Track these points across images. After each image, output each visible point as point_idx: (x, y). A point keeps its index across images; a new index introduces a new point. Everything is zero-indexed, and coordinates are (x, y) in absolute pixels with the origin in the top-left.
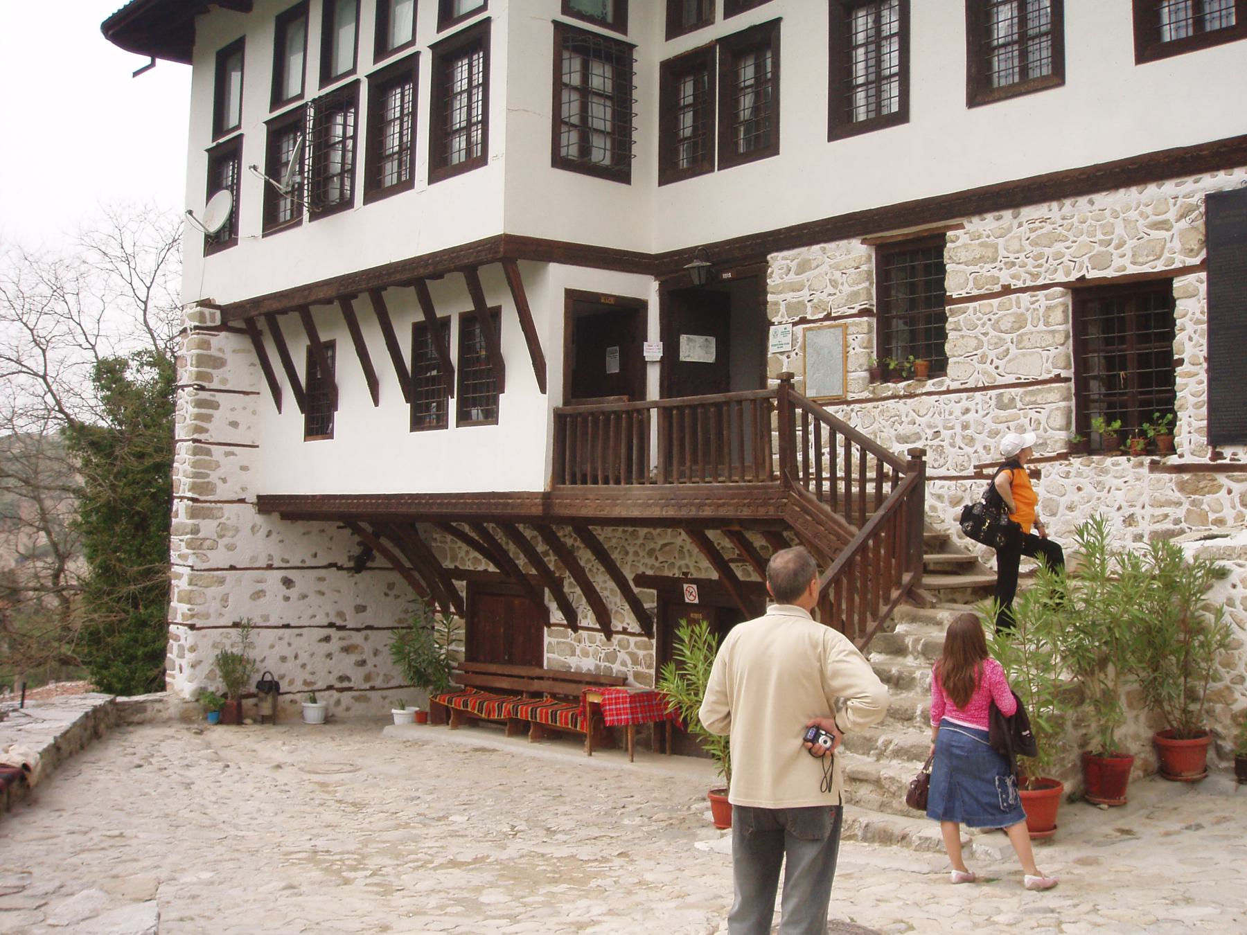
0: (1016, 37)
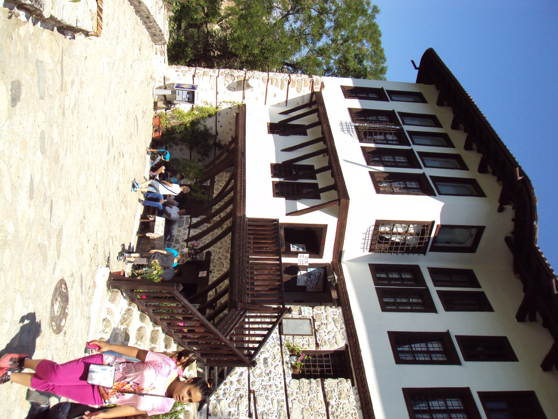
0: (432, 408)
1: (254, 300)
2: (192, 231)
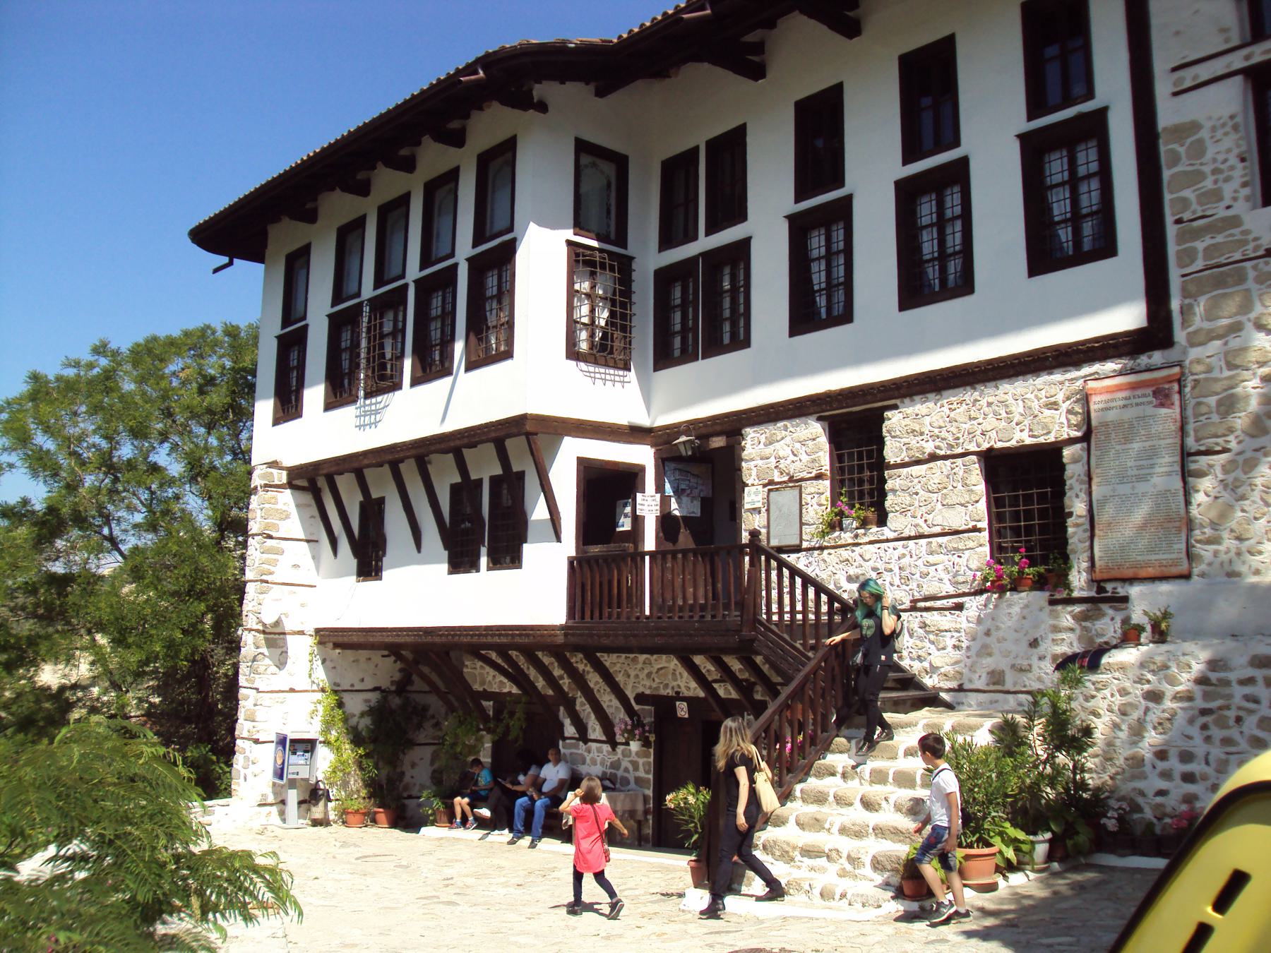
0: (936, 255)
1: (736, 603)
2: (592, 736)
